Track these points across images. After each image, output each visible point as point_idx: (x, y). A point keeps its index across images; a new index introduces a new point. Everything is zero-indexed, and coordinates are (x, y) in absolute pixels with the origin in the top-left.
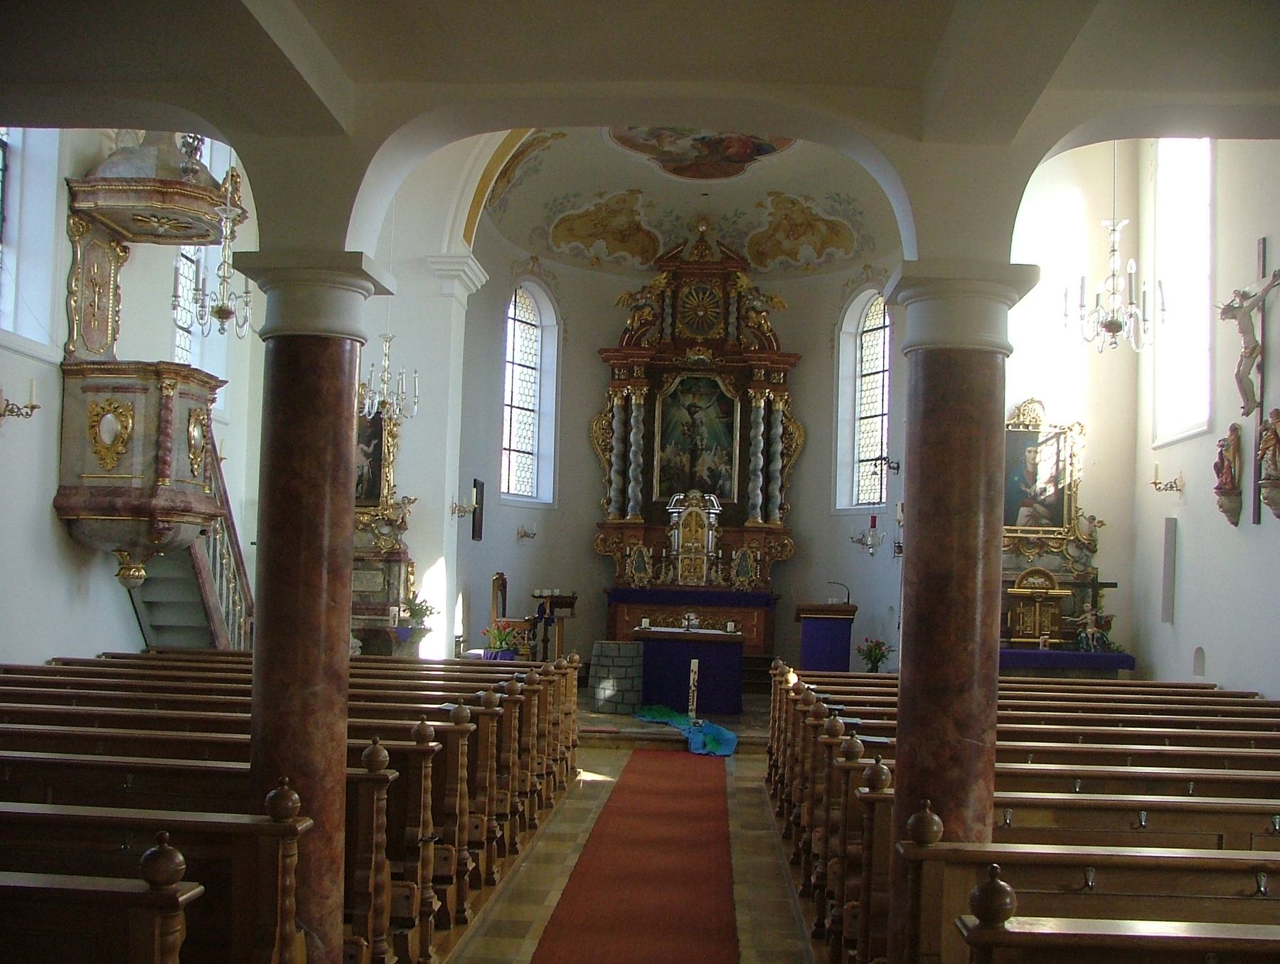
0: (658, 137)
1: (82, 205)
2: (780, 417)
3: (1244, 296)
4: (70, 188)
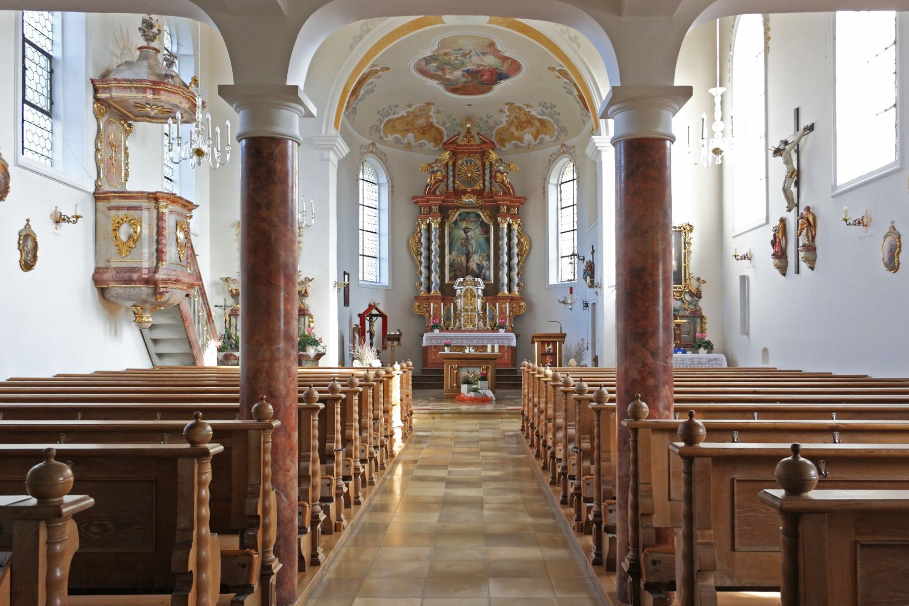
0: (443, 70)
1: (102, 95)
2: (516, 233)
3: (786, 143)
4: (94, 85)
